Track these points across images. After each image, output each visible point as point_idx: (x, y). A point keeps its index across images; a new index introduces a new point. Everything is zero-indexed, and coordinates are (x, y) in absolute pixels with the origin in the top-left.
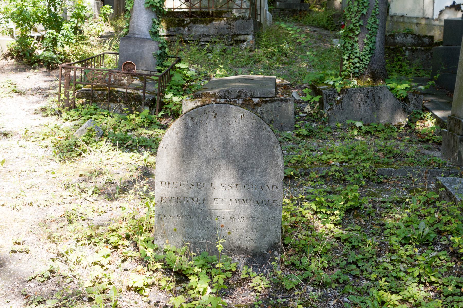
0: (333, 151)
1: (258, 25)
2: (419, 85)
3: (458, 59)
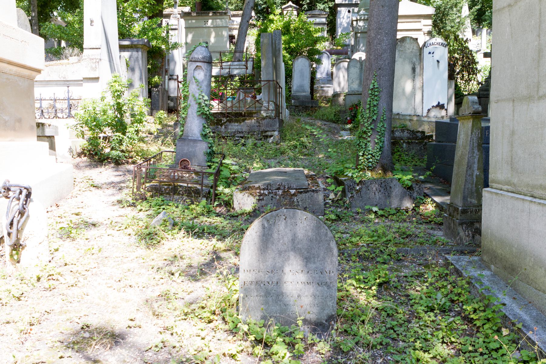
0: (361, 234)
1: (281, 122)
2: (420, 175)
3: (453, 159)
